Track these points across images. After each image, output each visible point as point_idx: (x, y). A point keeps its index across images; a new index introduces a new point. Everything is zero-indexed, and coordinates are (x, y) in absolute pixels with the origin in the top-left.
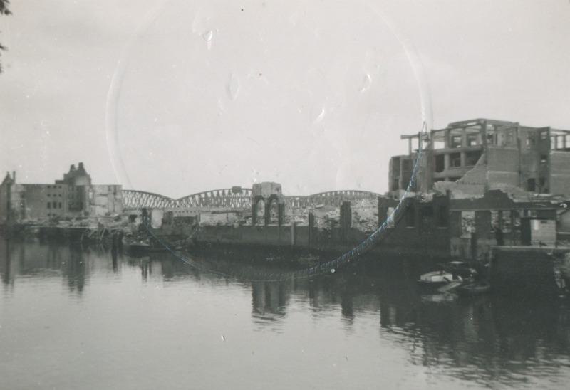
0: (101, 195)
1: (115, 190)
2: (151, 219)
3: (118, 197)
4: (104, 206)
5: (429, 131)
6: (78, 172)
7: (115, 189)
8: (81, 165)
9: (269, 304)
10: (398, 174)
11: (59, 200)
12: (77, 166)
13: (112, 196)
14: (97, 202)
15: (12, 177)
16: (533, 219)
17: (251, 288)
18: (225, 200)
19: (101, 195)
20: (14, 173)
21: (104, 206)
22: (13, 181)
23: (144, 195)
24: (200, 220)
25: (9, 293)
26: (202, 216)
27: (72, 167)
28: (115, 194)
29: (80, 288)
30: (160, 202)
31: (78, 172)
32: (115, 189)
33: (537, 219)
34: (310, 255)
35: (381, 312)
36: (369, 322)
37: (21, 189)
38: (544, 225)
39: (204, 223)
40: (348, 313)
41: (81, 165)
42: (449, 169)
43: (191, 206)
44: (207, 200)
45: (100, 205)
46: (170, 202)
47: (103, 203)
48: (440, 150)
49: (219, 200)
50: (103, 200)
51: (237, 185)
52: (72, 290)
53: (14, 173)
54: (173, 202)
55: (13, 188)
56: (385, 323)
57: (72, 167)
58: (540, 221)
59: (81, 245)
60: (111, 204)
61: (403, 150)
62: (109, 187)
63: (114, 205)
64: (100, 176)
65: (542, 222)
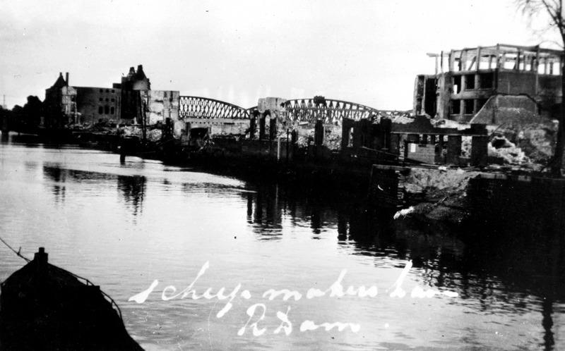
0: (157, 101)
1: (171, 96)
2: (173, 129)
3: (175, 104)
4: (159, 114)
5: (495, 44)
6: (138, 75)
7: (172, 95)
8: (140, 67)
9: (265, 219)
10: (422, 95)
11: (112, 105)
12: (136, 69)
13: (169, 103)
14: (152, 109)
15: (65, 78)
16: (412, 142)
17: (247, 201)
18: (326, 112)
19: (157, 101)
20: (67, 74)
21: (159, 114)
22: (66, 83)
23: (210, 102)
24: (210, 133)
25: (60, 204)
26: (212, 128)
27: (132, 69)
28: (171, 100)
29: (136, 201)
30: (228, 111)
31: (138, 75)
32: (172, 95)
33: (415, 143)
34: (542, 182)
35: (338, 225)
36: (331, 234)
37: (74, 92)
38: (422, 148)
39: (214, 135)
40: (317, 227)
41: (140, 67)
42: (465, 91)
43: (241, 115)
44: (414, 104)
45: (154, 112)
46: (240, 111)
47: (158, 111)
48: (485, 70)
49: (319, 111)
50: (159, 107)
51: (319, 94)
52: (128, 200)
53: (67, 74)
54: (242, 111)
55: (64, 90)
56: (342, 237)
57: (132, 69)
58: (418, 145)
59: (387, 167)
60: (166, 111)
61: (430, 72)
62: (165, 94)
63: (170, 113)
64: (159, 82)
65: (420, 146)
